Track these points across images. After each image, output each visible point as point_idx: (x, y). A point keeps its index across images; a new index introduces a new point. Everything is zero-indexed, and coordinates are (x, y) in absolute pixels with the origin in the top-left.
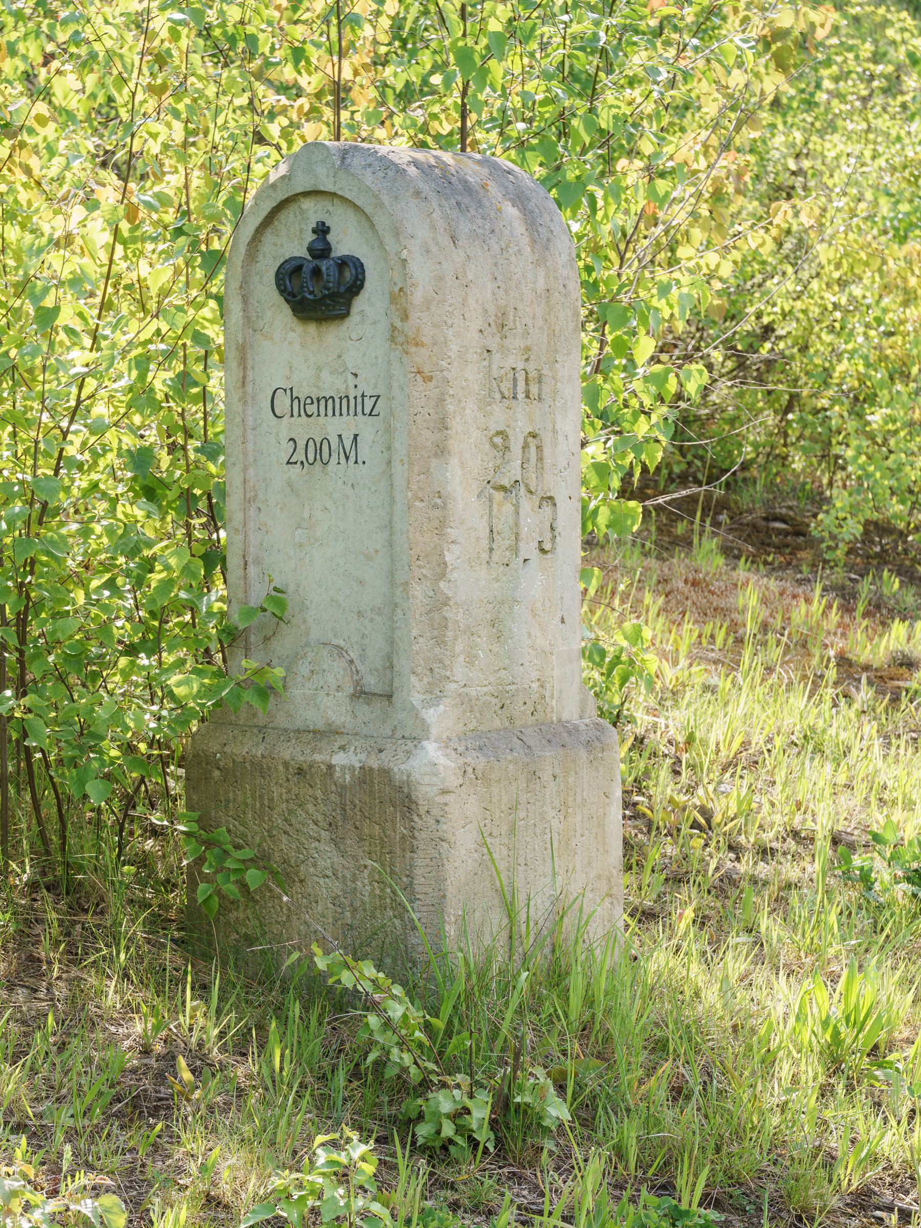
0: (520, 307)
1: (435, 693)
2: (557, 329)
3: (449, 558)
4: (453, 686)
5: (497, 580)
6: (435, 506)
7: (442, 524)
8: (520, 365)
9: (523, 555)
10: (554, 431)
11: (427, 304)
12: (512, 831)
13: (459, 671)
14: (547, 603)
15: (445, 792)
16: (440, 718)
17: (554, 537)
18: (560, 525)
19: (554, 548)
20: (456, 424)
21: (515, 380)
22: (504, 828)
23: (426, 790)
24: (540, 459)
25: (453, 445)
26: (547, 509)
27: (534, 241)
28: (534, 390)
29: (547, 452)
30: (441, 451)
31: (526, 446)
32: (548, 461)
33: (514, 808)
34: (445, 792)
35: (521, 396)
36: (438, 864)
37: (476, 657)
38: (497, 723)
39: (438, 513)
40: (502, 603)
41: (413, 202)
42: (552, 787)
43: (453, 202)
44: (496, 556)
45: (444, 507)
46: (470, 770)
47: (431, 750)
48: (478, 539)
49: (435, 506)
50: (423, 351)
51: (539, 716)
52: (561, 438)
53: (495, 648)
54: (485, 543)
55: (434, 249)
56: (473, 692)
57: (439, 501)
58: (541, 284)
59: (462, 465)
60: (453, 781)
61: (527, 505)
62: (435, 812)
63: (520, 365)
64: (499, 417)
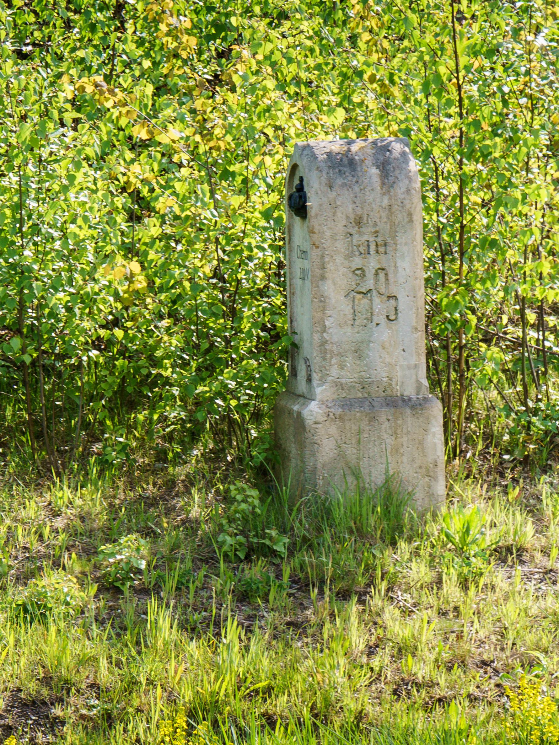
0: (371, 214)
1: (323, 380)
2: (397, 222)
3: (327, 323)
4: (331, 378)
5: (358, 333)
6: (321, 301)
7: (324, 309)
8: (372, 239)
9: (375, 321)
10: (396, 267)
11: (316, 215)
12: (359, 442)
13: (334, 371)
14: (393, 343)
15: (316, 423)
16: (322, 391)
17: (396, 314)
18: (400, 308)
19: (396, 319)
20: (330, 266)
21: (368, 246)
22: (354, 441)
23: (309, 421)
24: (387, 279)
25: (327, 275)
26: (392, 302)
27: (383, 184)
28: (382, 249)
29: (391, 276)
30: (323, 278)
31: (377, 274)
32: (391, 280)
33: (359, 432)
34: (316, 423)
35: (372, 252)
36: (313, 454)
37: (345, 366)
38: (360, 395)
39: (322, 304)
40: (362, 342)
41: (315, 172)
42: (386, 425)
43: (337, 170)
44: (357, 323)
45: (324, 302)
46: (331, 414)
47: (313, 406)
48: (345, 315)
49: (321, 301)
50: (315, 236)
51: (389, 392)
52: (400, 270)
53: (358, 362)
54: (350, 317)
55: (319, 192)
56: (343, 381)
57: (322, 301)
58: (386, 202)
59: (335, 284)
60: (321, 419)
61: (377, 300)
62: (312, 431)
63: (372, 239)
64: (358, 262)
